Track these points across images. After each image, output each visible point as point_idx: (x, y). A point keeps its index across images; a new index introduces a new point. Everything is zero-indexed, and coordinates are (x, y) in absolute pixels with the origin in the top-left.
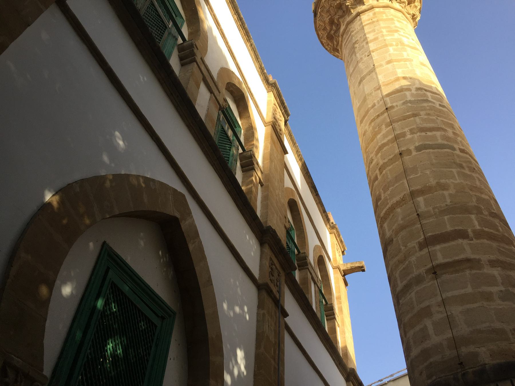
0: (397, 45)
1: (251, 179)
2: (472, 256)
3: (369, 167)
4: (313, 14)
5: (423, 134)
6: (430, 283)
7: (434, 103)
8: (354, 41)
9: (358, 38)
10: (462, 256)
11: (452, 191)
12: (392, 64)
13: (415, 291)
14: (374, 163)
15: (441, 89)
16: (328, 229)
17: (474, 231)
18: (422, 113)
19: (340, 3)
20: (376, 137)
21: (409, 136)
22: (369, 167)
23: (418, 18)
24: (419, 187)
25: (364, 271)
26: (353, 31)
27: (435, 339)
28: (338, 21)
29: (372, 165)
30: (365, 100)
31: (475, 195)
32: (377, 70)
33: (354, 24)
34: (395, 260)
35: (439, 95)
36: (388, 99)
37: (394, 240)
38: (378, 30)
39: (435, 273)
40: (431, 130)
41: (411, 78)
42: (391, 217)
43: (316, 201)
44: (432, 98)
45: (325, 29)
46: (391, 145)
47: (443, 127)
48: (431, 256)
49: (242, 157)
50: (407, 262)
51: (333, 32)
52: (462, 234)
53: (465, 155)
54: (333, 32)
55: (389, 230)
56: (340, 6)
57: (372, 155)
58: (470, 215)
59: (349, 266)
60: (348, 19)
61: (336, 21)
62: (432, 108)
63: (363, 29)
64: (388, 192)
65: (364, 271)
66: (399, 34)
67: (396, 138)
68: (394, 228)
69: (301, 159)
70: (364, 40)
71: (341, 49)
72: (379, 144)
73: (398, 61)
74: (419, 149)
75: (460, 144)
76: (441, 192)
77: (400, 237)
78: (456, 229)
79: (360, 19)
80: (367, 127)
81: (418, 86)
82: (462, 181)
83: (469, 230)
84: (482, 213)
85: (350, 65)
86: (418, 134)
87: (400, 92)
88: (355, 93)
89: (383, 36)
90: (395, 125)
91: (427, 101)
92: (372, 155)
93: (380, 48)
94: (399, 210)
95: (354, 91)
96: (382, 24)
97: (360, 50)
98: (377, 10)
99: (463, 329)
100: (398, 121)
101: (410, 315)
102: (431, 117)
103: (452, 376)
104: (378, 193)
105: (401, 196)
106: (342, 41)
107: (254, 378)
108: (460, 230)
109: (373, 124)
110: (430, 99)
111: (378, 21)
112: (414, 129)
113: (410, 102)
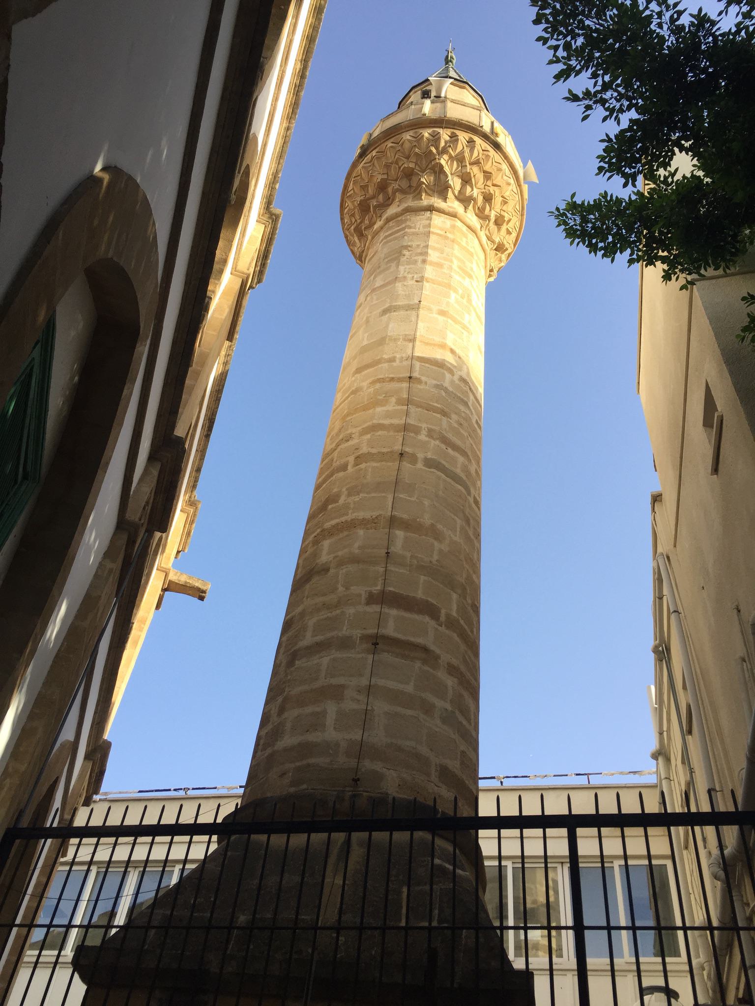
0: (462, 297)
2: (432, 647)
3: (338, 445)
5: (443, 446)
6: (360, 656)
9: (414, 244)
10: (419, 640)
11: (445, 547)
13: (332, 657)
14: (351, 443)
17: (448, 616)
18: (454, 417)
19: (413, 169)
21: (423, 437)
22: (338, 445)
24: (405, 516)
25: (202, 598)
26: (410, 227)
27: (330, 734)
28: (395, 192)
29: (346, 445)
30: (382, 342)
33: (418, 218)
34: (320, 600)
36: (417, 365)
37: (332, 571)
38: (447, 255)
39: (376, 644)
40: (456, 448)
41: (459, 357)
42: (341, 535)
44: (473, 404)
45: (364, 188)
47: (470, 454)
48: (380, 620)
50: (338, 612)
51: (374, 202)
52: (432, 611)
54: (374, 202)
55: (329, 553)
56: (409, 174)
58: (452, 592)
59: (183, 579)
60: (410, 203)
61: (390, 190)
62: (468, 419)
63: (428, 236)
64: (357, 499)
65: (202, 598)
67: (406, 428)
68: (340, 553)
70: (421, 254)
71: (373, 238)
72: (375, 421)
74: (429, 463)
76: (432, 540)
77: (344, 571)
78: (427, 601)
79: (430, 219)
80: (365, 384)
81: (463, 374)
83: (443, 612)
84: (465, 598)
85: (380, 273)
86: (437, 442)
88: (367, 321)
89: (450, 268)
90: (412, 409)
91: (466, 404)
92: (354, 430)
93: (439, 284)
94: (361, 532)
95: (368, 318)
96: (457, 251)
97: (408, 263)
98: (459, 224)
99: (378, 736)
100: (418, 406)
101: (306, 687)
103: (335, 793)
104: (335, 490)
105: (375, 514)
106: (382, 228)
108: (432, 604)
109: (378, 386)
110: (470, 404)
111: (453, 241)
113: (446, 390)
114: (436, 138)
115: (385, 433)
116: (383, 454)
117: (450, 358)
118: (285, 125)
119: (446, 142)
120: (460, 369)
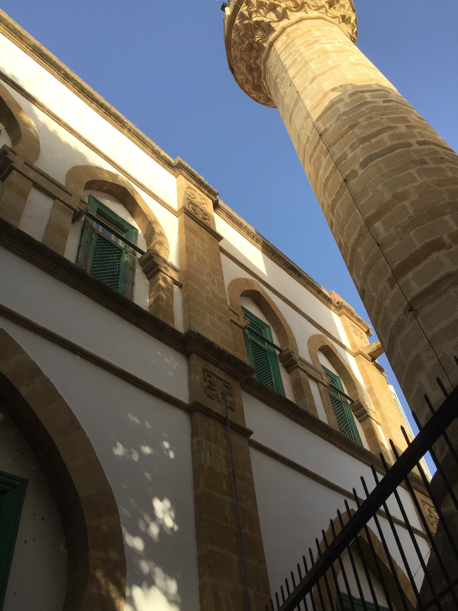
1: (158, 283)
4: (230, 72)
5: (367, 144)
7: (375, 102)
8: (274, 78)
10: (441, 274)
11: (414, 197)
12: (316, 81)
15: (386, 83)
16: (333, 311)
17: (451, 236)
18: (361, 120)
20: (318, 174)
21: (350, 155)
23: (353, 18)
24: (373, 211)
26: (271, 67)
31: (447, 190)
32: (302, 96)
33: (270, 58)
35: (382, 90)
36: (320, 124)
39: (412, 309)
40: (375, 135)
41: (341, 86)
43: (301, 283)
45: (247, 81)
46: (334, 175)
47: (392, 124)
49: (142, 263)
50: (383, 310)
53: (427, 146)
56: (251, 47)
57: (322, 198)
60: (263, 56)
62: (376, 109)
63: (280, 58)
66: (320, 43)
69: (258, 241)
72: (323, 181)
73: (323, 73)
74: (364, 165)
75: (419, 137)
78: (426, 243)
81: (351, 91)
82: (426, 179)
83: (445, 237)
87: (331, 108)
89: (301, 54)
90: (334, 149)
91: (366, 103)
93: (301, 70)
96: (297, 42)
97: (282, 83)
98: (289, 30)
100: (335, 144)
102: (373, 120)
105: (357, 231)
107: (196, 528)
108: (432, 242)
110: (369, 99)
111: (292, 41)
112: (354, 143)
113: (345, 114)
114: (243, 16)
115: (331, 180)
116: (338, 192)
117: (334, 95)
118: (126, 131)
119: (247, 10)
120: (346, 91)
